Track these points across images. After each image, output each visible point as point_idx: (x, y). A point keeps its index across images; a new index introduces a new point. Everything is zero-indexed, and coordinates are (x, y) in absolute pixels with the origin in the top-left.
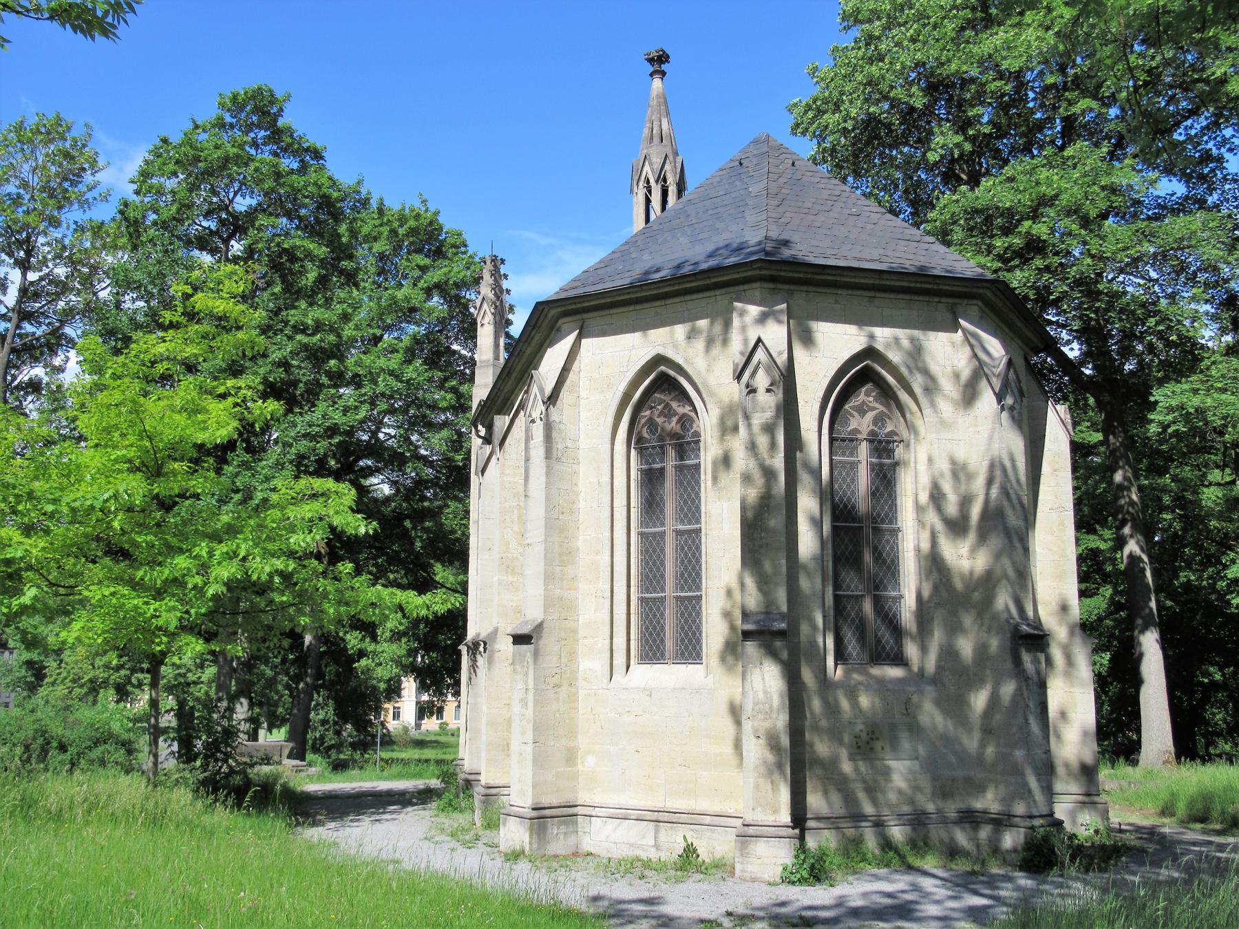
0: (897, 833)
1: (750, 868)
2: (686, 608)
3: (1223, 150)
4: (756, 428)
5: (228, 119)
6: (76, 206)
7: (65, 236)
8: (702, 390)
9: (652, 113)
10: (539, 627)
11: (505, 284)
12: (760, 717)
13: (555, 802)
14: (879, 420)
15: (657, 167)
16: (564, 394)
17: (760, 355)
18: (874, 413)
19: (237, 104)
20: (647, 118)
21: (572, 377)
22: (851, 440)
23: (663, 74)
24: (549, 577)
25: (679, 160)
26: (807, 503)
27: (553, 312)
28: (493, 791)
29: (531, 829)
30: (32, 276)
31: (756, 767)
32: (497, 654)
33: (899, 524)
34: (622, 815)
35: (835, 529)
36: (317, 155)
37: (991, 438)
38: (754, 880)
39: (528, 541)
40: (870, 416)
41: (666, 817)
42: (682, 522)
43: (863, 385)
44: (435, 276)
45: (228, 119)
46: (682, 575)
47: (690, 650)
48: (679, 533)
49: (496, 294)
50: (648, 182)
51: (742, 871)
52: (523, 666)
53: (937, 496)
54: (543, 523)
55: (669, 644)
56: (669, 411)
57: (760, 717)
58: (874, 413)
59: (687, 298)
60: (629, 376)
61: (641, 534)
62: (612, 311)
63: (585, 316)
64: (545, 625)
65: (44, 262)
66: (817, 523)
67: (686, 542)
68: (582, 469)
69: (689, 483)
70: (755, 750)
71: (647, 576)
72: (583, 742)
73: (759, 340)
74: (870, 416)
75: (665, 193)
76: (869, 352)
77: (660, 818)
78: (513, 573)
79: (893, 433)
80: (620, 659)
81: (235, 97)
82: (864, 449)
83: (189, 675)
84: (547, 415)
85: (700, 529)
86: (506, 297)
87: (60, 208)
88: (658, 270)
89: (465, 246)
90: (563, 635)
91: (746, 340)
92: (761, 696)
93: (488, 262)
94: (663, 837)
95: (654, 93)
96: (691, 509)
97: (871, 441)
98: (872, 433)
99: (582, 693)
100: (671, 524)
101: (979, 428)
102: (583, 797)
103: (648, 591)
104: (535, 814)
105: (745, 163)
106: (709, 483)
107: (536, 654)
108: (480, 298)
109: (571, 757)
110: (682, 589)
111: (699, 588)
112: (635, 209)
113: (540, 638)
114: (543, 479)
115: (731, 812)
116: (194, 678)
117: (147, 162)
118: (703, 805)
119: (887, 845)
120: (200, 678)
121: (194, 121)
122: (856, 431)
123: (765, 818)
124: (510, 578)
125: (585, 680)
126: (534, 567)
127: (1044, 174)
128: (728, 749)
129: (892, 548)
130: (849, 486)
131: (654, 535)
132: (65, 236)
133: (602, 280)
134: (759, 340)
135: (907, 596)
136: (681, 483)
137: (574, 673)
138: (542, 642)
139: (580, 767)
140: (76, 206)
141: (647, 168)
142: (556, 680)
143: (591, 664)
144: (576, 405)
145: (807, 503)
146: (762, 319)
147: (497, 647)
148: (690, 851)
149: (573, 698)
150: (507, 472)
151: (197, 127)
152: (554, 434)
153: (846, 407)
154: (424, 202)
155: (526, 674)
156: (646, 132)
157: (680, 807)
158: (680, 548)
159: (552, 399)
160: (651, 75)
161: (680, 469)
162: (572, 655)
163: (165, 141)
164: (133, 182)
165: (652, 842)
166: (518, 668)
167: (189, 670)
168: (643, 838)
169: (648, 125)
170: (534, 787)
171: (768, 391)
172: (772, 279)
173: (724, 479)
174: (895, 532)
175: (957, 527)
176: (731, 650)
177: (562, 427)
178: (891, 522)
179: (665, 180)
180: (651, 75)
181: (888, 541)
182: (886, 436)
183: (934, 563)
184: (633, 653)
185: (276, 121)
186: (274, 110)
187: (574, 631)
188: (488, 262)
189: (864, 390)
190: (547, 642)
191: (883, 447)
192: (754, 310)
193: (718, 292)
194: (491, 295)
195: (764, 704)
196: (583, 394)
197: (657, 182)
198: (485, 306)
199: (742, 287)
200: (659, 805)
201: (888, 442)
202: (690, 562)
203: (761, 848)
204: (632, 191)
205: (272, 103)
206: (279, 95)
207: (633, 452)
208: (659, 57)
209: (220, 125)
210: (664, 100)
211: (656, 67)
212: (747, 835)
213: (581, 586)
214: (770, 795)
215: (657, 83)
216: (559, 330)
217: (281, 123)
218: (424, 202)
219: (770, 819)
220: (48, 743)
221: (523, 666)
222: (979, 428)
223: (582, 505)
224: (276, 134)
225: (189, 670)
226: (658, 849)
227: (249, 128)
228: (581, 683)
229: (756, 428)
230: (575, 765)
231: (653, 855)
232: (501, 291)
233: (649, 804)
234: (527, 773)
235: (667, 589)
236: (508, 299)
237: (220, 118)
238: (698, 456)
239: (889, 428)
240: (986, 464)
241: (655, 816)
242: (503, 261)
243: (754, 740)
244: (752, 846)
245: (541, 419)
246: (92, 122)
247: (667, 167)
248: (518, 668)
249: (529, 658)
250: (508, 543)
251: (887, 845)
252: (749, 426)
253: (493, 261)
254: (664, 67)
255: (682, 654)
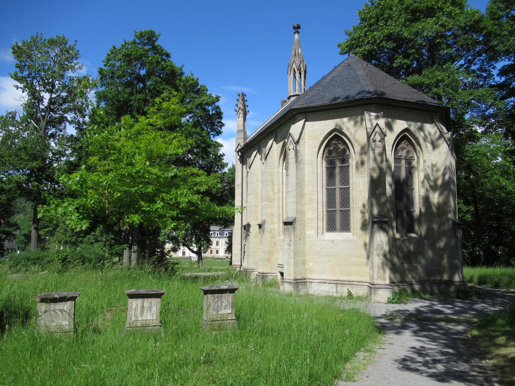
0: (417, 287)
1: (377, 298)
2: (344, 214)
3: (490, 68)
4: (376, 154)
5: (137, 41)
6: (70, 71)
7: (66, 81)
8: (353, 142)
9: (295, 46)
10: (295, 219)
11: (246, 104)
12: (379, 249)
13: (300, 278)
14: (408, 152)
15: (298, 65)
16: (301, 141)
17: (377, 129)
18: (407, 150)
19: (141, 35)
20: (293, 48)
21: (303, 135)
22: (399, 159)
23: (299, 32)
24: (297, 203)
25: (305, 63)
26: (389, 179)
27: (295, 113)
28: (265, 275)
29: (294, 287)
30: (54, 96)
31: (378, 266)
32: (265, 229)
33: (413, 187)
34: (323, 282)
35: (396, 188)
36: (168, 56)
37: (445, 160)
38: (378, 302)
39: (289, 190)
40: (405, 151)
41: (340, 282)
42: (342, 185)
43: (403, 141)
44: (198, 101)
45: (137, 41)
46: (342, 203)
47: (346, 227)
48: (340, 189)
49: (244, 107)
50: (294, 70)
51: (374, 299)
52: (289, 233)
53: (427, 177)
54: (295, 184)
55: (338, 226)
56: (337, 147)
57: (379, 249)
58: (407, 150)
59: (347, 109)
60: (324, 135)
61: (327, 189)
62: (317, 113)
63: (307, 114)
64: (297, 219)
65: (57, 91)
66: (391, 185)
67: (343, 192)
68: (306, 167)
69: (344, 172)
70: (377, 260)
71: (329, 203)
72: (307, 258)
73: (377, 124)
74: (405, 151)
75: (300, 74)
76: (406, 130)
77: (337, 283)
78: (270, 202)
79: (412, 157)
80: (320, 231)
81: (141, 34)
82: (403, 162)
83: (98, 238)
84: (296, 148)
85: (336, 188)
86: (247, 108)
87: (65, 71)
88: (339, 98)
89: (207, 91)
90: (301, 222)
91: (372, 124)
92: (379, 242)
93: (241, 96)
94: (339, 289)
95: (296, 39)
96: (345, 180)
97: (405, 159)
98: (406, 157)
99: (307, 242)
100: (338, 186)
101: (441, 156)
102: (308, 276)
103: (329, 208)
104: (295, 282)
105: (350, 64)
106: (354, 172)
107: (294, 229)
108: (238, 108)
109: (304, 263)
110: (342, 208)
111: (349, 207)
112: (289, 79)
113: (295, 223)
114: (295, 169)
115: (363, 280)
116: (100, 240)
117: (108, 55)
118: (353, 278)
119: (414, 292)
120: (102, 239)
121: (125, 41)
122: (401, 156)
123: (381, 282)
124: (269, 204)
125: (308, 237)
126: (292, 199)
127: (437, 73)
128: (364, 260)
129: (411, 195)
130: (398, 174)
131: (332, 189)
132: (66, 81)
133: (313, 102)
134: (377, 124)
135: (416, 210)
136: (341, 172)
137: (305, 235)
138: (296, 225)
139: (307, 266)
140: (70, 71)
141: (294, 65)
142: (299, 237)
143: (310, 232)
144: (304, 145)
145: (389, 179)
146: (377, 117)
147: (265, 226)
148: (350, 294)
149: (304, 243)
150: (268, 167)
151: (126, 43)
152: (298, 154)
153: (398, 148)
154: (192, 75)
155: (290, 235)
156: (293, 52)
157: (342, 279)
158: (341, 194)
159: (298, 142)
160: (294, 33)
161: (341, 167)
162: (304, 228)
163: (114, 47)
164: (103, 62)
165: (335, 291)
166: (286, 233)
167: (98, 237)
168: (332, 289)
169: (294, 50)
170: (294, 272)
171: (380, 141)
172: (377, 104)
173: (361, 169)
174: (412, 189)
175: (434, 188)
176: (364, 227)
177: (300, 152)
178: (411, 187)
179: (300, 70)
180: (294, 33)
181: (410, 193)
182: (410, 158)
183: (426, 200)
184: (324, 229)
185: (154, 43)
186: (154, 39)
187: (304, 221)
188: (241, 96)
189: (403, 142)
190: (297, 224)
191: (409, 162)
192: (373, 114)
193: (358, 107)
194: (242, 107)
195: (380, 245)
196: (306, 141)
197: (298, 70)
198: (240, 111)
199: (367, 106)
200: (337, 278)
201: (410, 160)
202: (345, 198)
203: (380, 292)
204: (288, 73)
205: (153, 37)
206: (157, 33)
207: (324, 161)
208: (297, 27)
209: (134, 42)
210: (299, 41)
211: (296, 30)
212: (373, 287)
213: (306, 206)
214: (383, 275)
215: (296, 36)
216: (295, 119)
217: (156, 44)
218: (192, 75)
219: (383, 283)
220: (85, 260)
221: (289, 233)
222: (441, 156)
223: (306, 179)
224: (154, 48)
225: (98, 237)
226: (337, 293)
227: (145, 44)
228: (307, 238)
229: (376, 154)
230: (305, 265)
231: (335, 295)
232: (245, 106)
233: (333, 278)
234: (292, 269)
235: (337, 207)
236: (247, 109)
237: (134, 41)
238: (348, 163)
239: (410, 155)
240: (443, 168)
241: (336, 282)
242: (245, 95)
243: (377, 257)
244: (377, 292)
245: (293, 149)
246: (18, 42)
247: (301, 65)
248: (286, 233)
249: (291, 229)
250: (268, 192)
251: (414, 292)
252: (374, 153)
253: (242, 95)
254: (299, 30)
255: (342, 229)
